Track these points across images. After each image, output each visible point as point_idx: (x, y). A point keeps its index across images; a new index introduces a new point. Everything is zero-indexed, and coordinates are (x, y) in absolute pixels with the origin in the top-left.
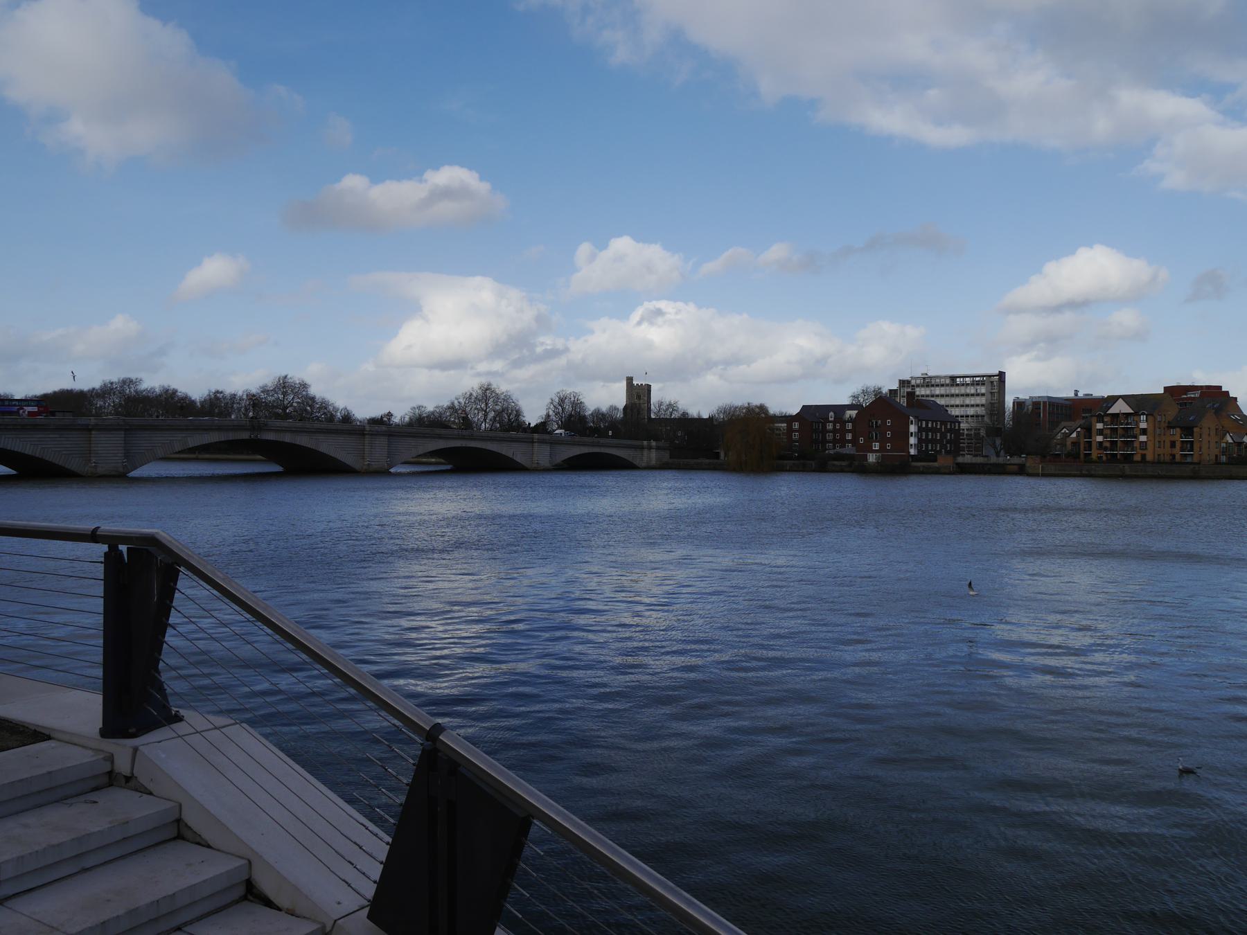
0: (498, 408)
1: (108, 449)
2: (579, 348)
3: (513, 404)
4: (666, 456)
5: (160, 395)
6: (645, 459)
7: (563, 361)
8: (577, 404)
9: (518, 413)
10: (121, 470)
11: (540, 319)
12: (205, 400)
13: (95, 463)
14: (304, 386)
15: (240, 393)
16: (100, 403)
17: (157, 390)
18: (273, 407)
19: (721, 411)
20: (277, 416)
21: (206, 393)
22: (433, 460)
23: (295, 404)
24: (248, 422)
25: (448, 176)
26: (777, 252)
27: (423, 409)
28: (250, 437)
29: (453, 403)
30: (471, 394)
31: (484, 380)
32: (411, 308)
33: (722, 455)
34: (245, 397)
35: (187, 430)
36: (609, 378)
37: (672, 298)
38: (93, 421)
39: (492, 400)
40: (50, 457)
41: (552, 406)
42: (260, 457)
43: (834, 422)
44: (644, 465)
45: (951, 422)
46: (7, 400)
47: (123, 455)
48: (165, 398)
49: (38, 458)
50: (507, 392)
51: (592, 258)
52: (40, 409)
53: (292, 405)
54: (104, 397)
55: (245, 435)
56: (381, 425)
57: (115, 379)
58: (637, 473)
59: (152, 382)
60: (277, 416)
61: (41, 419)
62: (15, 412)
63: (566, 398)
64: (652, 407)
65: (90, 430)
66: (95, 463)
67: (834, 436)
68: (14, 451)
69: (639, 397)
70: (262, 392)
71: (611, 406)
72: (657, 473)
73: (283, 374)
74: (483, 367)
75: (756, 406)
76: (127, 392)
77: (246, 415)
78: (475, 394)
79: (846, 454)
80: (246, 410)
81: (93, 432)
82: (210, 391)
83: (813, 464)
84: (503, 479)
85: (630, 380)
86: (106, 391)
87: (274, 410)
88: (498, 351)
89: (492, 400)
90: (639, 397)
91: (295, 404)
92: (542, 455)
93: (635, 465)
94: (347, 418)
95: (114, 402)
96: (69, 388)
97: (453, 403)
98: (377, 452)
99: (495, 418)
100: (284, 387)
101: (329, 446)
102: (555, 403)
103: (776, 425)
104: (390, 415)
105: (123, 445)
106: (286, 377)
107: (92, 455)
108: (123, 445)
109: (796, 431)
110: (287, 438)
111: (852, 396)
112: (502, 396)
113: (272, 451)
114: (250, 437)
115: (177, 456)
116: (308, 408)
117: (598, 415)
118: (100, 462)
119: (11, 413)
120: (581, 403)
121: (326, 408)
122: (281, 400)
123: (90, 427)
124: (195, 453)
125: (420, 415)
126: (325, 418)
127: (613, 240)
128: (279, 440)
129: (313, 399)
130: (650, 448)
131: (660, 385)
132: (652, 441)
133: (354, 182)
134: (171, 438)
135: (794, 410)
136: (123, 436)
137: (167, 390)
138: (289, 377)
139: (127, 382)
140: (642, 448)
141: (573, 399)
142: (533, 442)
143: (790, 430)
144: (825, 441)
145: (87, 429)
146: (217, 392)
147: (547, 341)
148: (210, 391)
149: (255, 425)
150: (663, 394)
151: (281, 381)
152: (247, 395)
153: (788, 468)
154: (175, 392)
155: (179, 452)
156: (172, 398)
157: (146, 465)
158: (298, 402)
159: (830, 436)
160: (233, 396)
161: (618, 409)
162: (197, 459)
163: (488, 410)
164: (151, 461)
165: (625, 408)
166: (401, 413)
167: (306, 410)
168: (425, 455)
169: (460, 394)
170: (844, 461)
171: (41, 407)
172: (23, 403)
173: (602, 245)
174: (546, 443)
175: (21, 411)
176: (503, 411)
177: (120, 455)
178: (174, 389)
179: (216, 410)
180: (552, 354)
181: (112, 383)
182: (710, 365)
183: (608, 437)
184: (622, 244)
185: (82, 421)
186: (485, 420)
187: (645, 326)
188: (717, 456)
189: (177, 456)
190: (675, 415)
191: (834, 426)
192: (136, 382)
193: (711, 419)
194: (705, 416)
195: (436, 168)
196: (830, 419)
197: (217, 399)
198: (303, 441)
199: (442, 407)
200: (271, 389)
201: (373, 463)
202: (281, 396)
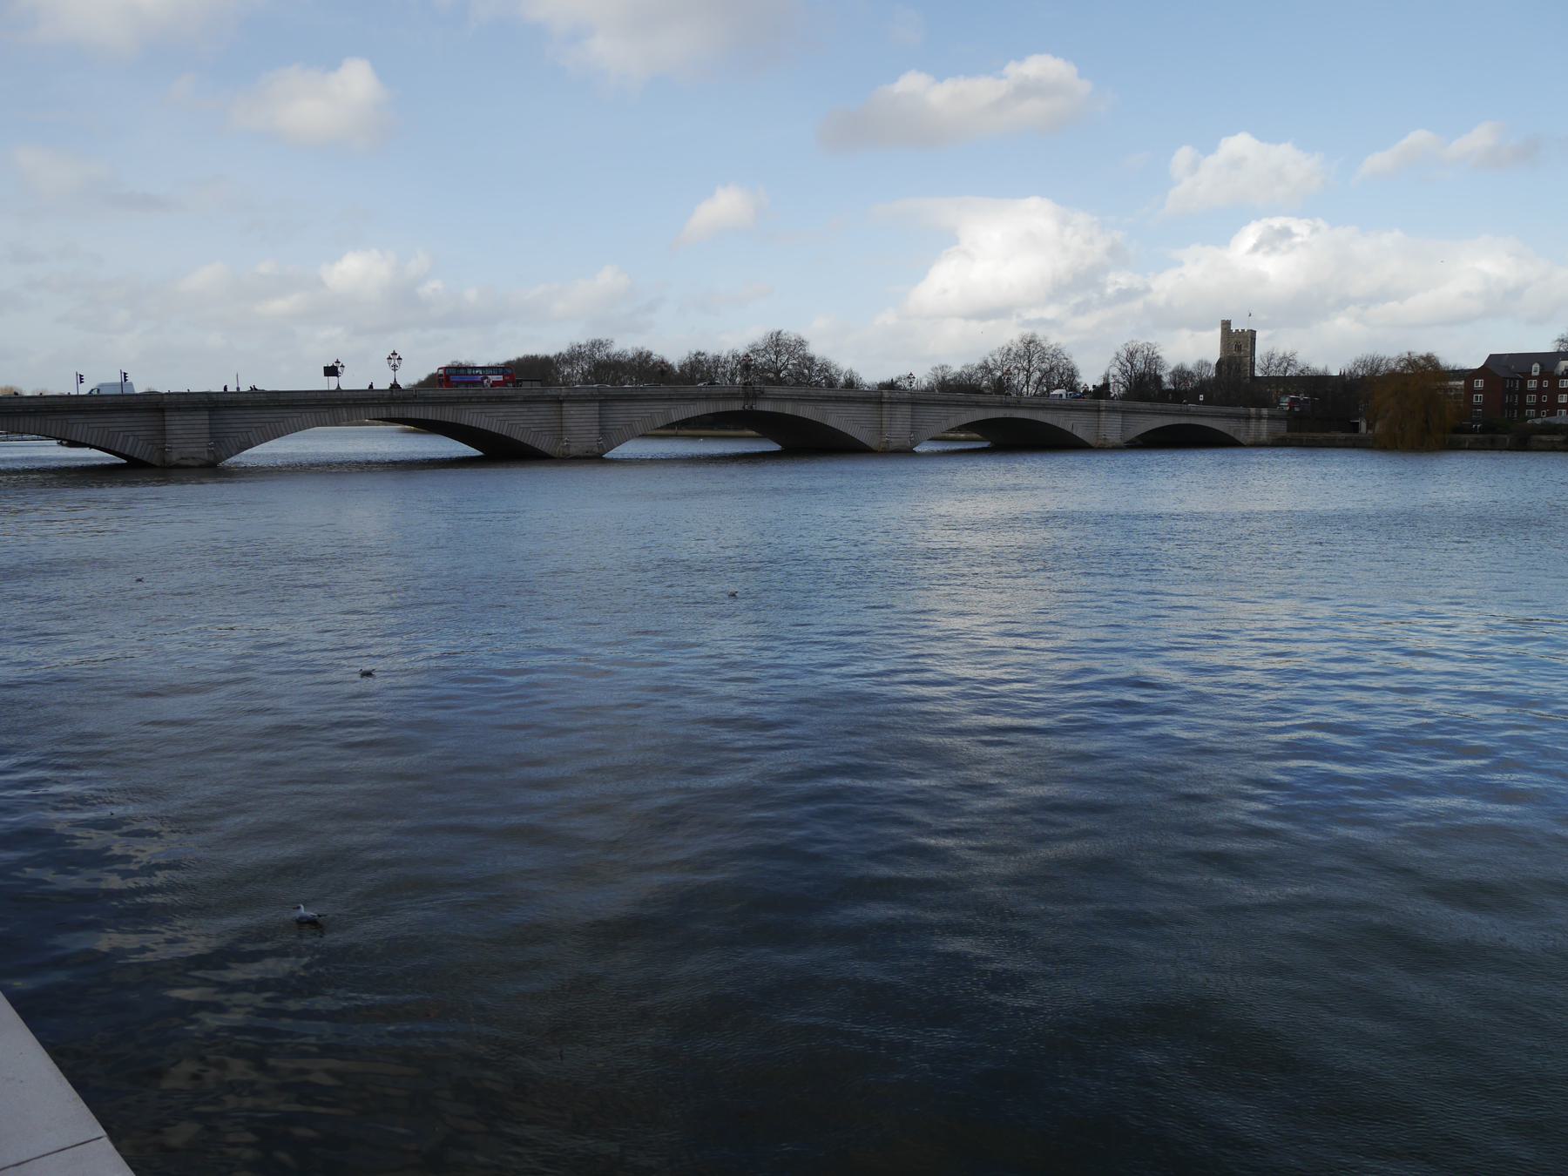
0: (1044, 366)
1: (581, 423)
2: (1165, 285)
3: (1065, 361)
4: (1282, 429)
5: (633, 360)
6: (1252, 433)
7: (1138, 305)
8: (1152, 360)
9: (1073, 373)
10: (596, 450)
11: (1114, 251)
12: (685, 365)
13: (567, 441)
14: (801, 343)
15: (724, 354)
16: (567, 370)
17: (630, 353)
18: (764, 370)
19: (1359, 366)
20: (769, 381)
21: (686, 354)
22: (962, 435)
23: (790, 367)
24: (741, 389)
25: (1039, 67)
26: (1480, 137)
27: (947, 370)
28: (744, 407)
29: (986, 362)
30: (1010, 350)
31: (1028, 331)
32: (945, 241)
33: (1363, 426)
34: (730, 359)
35: (671, 400)
36: (1198, 326)
37: (1300, 216)
38: (564, 391)
39: (1037, 355)
40: (517, 435)
41: (1117, 363)
42: (754, 433)
43: (1540, 378)
44: (1249, 440)
45: (1511, 379)
46: (470, 368)
47: (598, 432)
48: (639, 363)
49: (505, 437)
50: (1056, 344)
51: (1194, 167)
52: (507, 378)
53: (786, 368)
54: (571, 363)
55: (737, 406)
56: (889, 395)
57: (583, 342)
58: (1236, 451)
59: (625, 344)
60: (769, 381)
61: (509, 390)
62: (479, 382)
63: (1136, 352)
64: (1258, 361)
65: (561, 402)
66: (567, 441)
67: (1539, 399)
68: (479, 428)
69: (1239, 348)
70: (752, 352)
71: (1201, 361)
72: (1265, 452)
73: (777, 329)
74: (1033, 314)
75: (1422, 357)
76: (597, 356)
77: (732, 381)
78: (1014, 349)
79: (1561, 425)
80: (732, 374)
81: (564, 405)
82: (690, 353)
83: (1508, 440)
84: (1218, 455)
85: (1226, 325)
86: (572, 358)
87: (765, 374)
88: (1058, 291)
89: (1037, 355)
90: (1239, 348)
91: (790, 367)
92: (1112, 427)
93: (1237, 441)
94: (850, 384)
95: (582, 369)
96: (534, 355)
97: (986, 362)
98: (898, 425)
99: (1040, 379)
100: (777, 345)
101: (838, 419)
102: (1122, 359)
103: (1452, 383)
104: (910, 377)
105: (597, 420)
106: (779, 333)
107: (564, 432)
108: (597, 420)
109: (1479, 392)
110: (788, 409)
111: (1559, 340)
112: (1050, 351)
113: (767, 424)
114: (744, 407)
115: (662, 432)
116: (806, 371)
117: (1181, 375)
118: (571, 440)
119: (475, 383)
120: (1158, 357)
121: (827, 371)
122: (773, 362)
123: (561, 399)
124: (674, 428)
125: (943, 378)
126: (825, 383)
127: (1223, 140)
128: (778, 411)
129: (811, 359)
130: (1259, 417)
131: (1268, 333)
132: (392, 408)
133: (912, 83)
134: (652, 411)
135: (1476, 362)
136: (597, 408)
137: (641, 353)
138: (783, 333)
139: (597, 345)
140: (1248, 418)
141: (1146, 352)
142: (1099, 411)
143: (1470, 390)
144: (1523, 406)
145: (559, 401)
146: (699, 354)
147: (1119, 280)
148: (690, 353)
149: (749, 393)
150: (1273, 348)
151: (774, 338)
152: (733, 357)
153: (1467, 445)
154: (649, 355)
155: (662, 428)
156: (647, 363)
157: (276, 440)
158: (794, 364)
159: (1531, 399)
160: (717, 359)
161: (1210, 365)
162: (676, 436)
163: (1031, 369)
164: (630, 439)
165: (1219, 364)
166: (923, 376)
167: (803, 374)
168: (952, 430)
169: (996, 348)
170: (1556, 434)
171: (507, 375)
172: (487, 372)
173: (1209, 147)
174: (1117, 411)
175: (485, 381)
176: (1052, 369)
177: (594, 432)
178: (648, 352)
179: (698, 376)
180: (1126, 295)
181: (580, 347)
182: (1343, 303)
183: (1198, 402)
184: (1240, 144)
185: (552, 391)
186: (1027, 382)
187: (1258, 256)
188: (1356, 428)
189: (662, 432)
190: (1291, 372)
191: (1540, 384)
192: (605, 345)
193: (1342, 377)
194: (1335, 373)
195: (1021, 58)
196: (1533, 374)
197: (699, 362)
198: (807, 412)
199: (972, 366)
200: (763, 348)
201: (892, 440)
202: (773, 357)
